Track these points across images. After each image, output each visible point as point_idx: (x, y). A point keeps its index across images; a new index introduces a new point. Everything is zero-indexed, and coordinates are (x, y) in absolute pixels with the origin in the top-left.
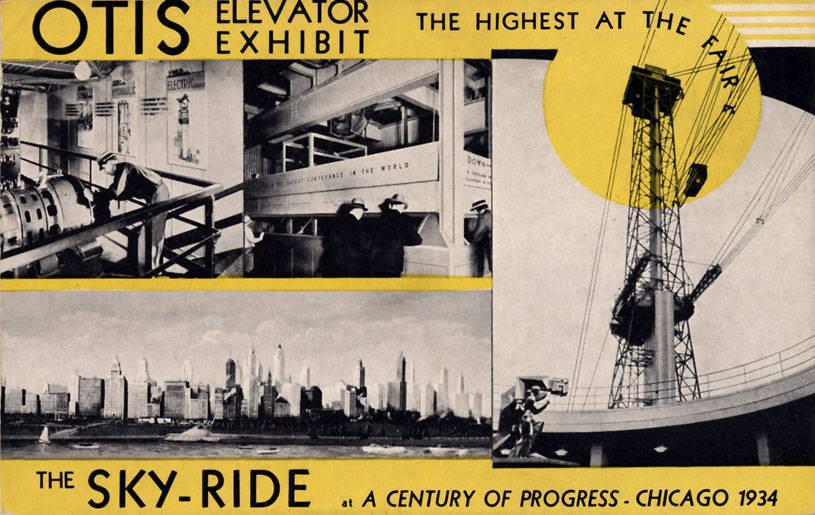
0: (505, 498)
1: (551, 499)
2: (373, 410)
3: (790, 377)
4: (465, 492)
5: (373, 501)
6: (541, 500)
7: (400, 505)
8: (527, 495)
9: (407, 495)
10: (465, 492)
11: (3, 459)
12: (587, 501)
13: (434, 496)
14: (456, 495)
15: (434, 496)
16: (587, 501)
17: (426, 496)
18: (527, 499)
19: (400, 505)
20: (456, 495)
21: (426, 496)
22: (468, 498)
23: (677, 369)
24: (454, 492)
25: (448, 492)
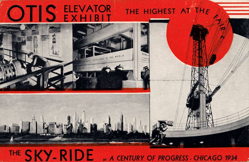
1: (168, 158)
10: (141, 156)
13: (132, 158)
21: (129, 157)
22: (142, 158)
23: (207, 118)
24: (138, 156)
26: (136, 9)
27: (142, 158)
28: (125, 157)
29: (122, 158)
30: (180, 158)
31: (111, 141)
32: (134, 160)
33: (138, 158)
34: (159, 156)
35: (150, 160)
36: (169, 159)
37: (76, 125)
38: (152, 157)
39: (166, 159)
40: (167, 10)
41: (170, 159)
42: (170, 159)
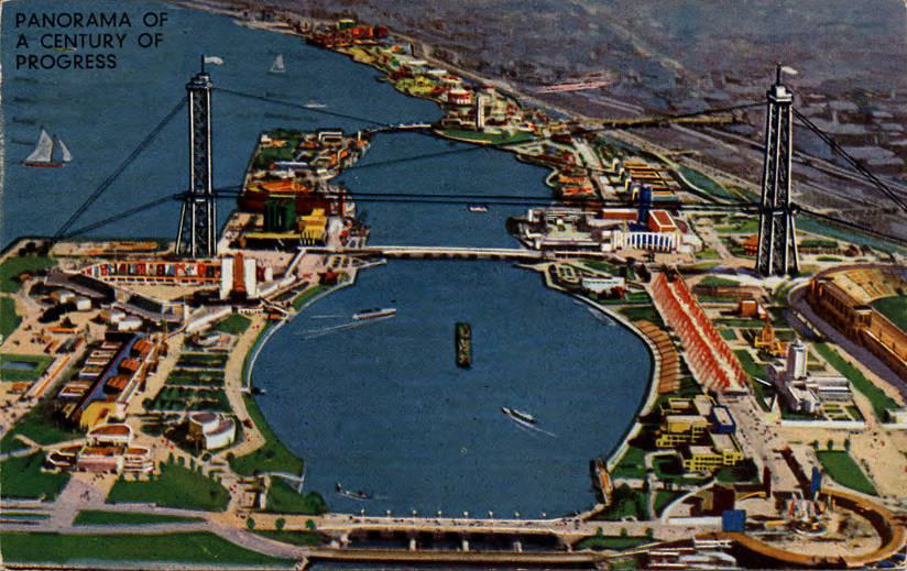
0: (157, 40)
1: (48, 62)
2: (692, 510)
3: (881, 346)
4: (117, 35)
5: (128, 22)
6: (38, 64)
7: (56, 46)
8: (21, 60)
9: (63, 38)
10: (117, 35)
11: (3, 380)
12: (84, 64)
13: (87, 39)
14: (108, 38)
15: (87, 39)
16: (84, 64)
17: (79, 38)
18: (355, 17)
19: (56, 46)
20: (108, 38)
21: (79, 38)
22: (121, 41)
23: (560, 217)
24: (105, 36)
25: (99, 36)
26: (88, 56)
27: (121, 41)
28: (67, 37)
29: (56, 41)
30: (88, 61)
31: (26, 371)
32: (97, 46)
33: (108, 43)
34: (18, 15)
35: (149, 45)
36: (53, 64)
37: (199, 316)
38: (157, 18)
39: (43, 65)
40: (94, 58)
41: (56, 58)
42: (56, 58)
